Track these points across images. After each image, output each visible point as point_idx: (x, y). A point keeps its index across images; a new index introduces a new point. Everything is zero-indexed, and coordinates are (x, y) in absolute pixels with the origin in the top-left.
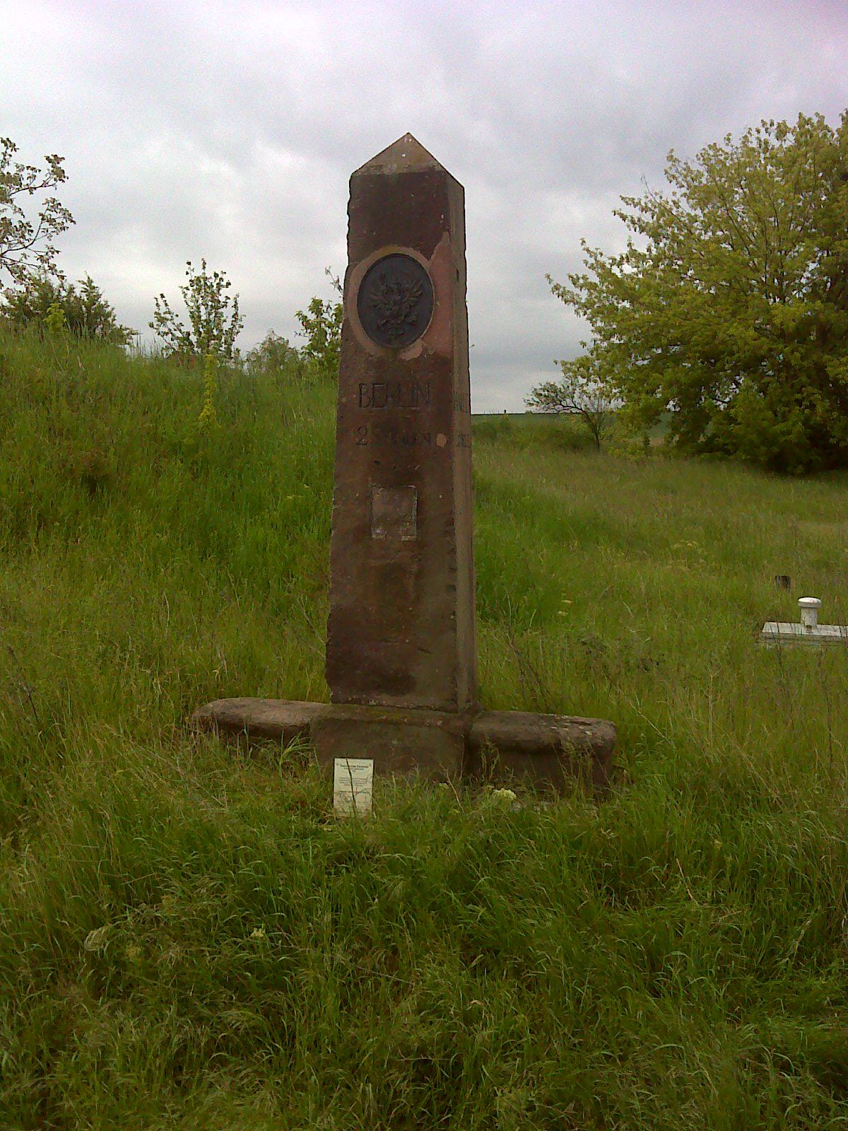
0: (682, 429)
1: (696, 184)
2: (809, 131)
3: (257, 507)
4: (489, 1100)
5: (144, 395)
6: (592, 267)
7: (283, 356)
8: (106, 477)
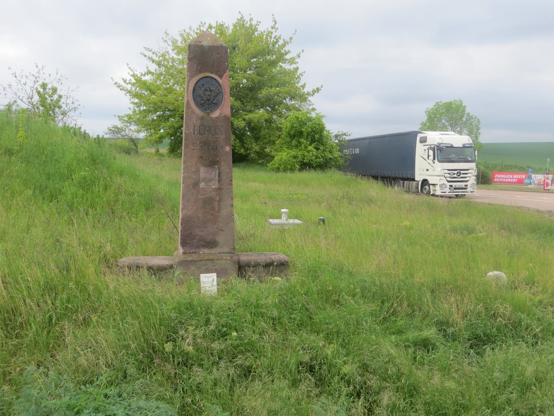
2: (221, 28)
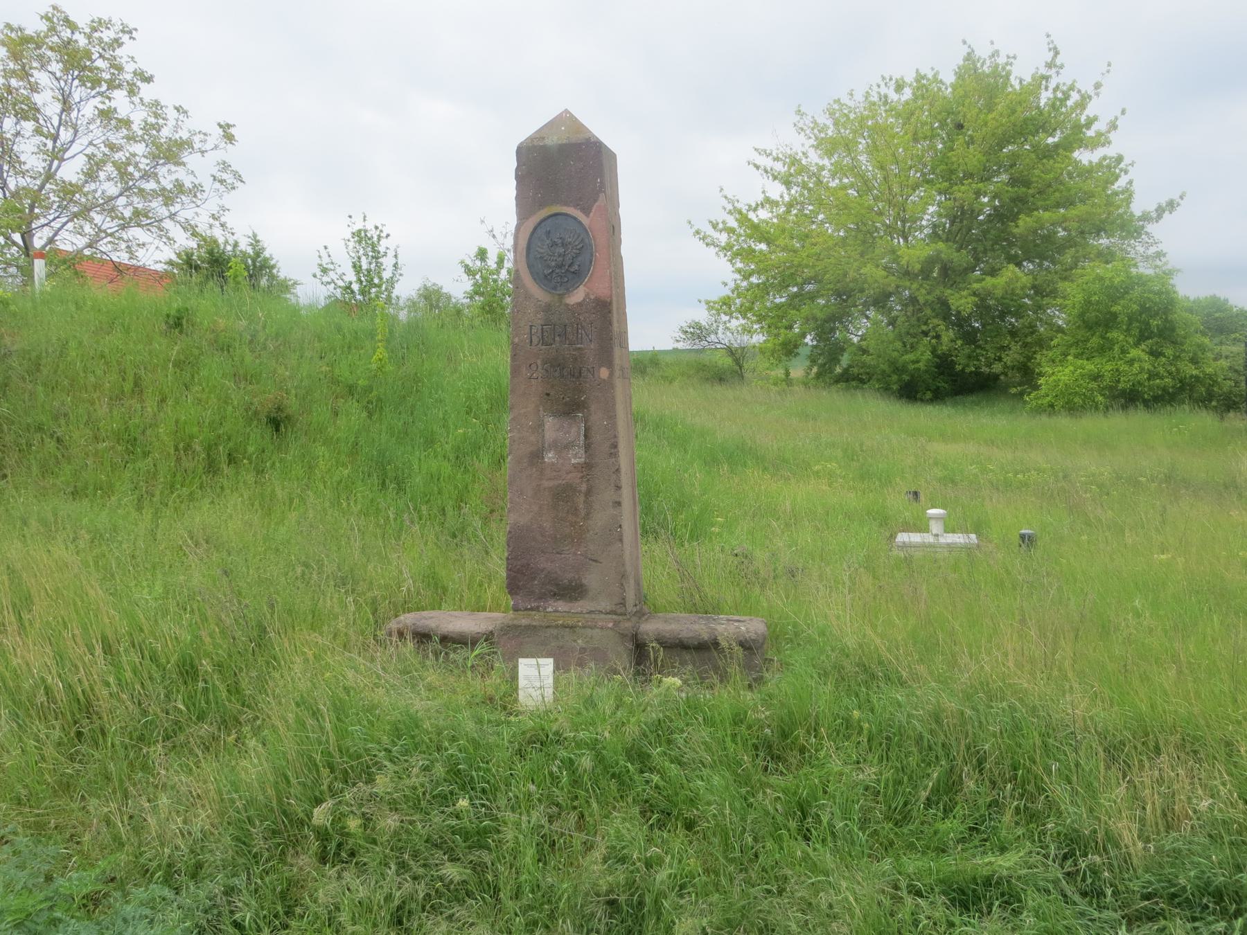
0: (820, 361)
1: (823, 135)
5: (320, 341)
6: (730, 213)
7: (438, 300)
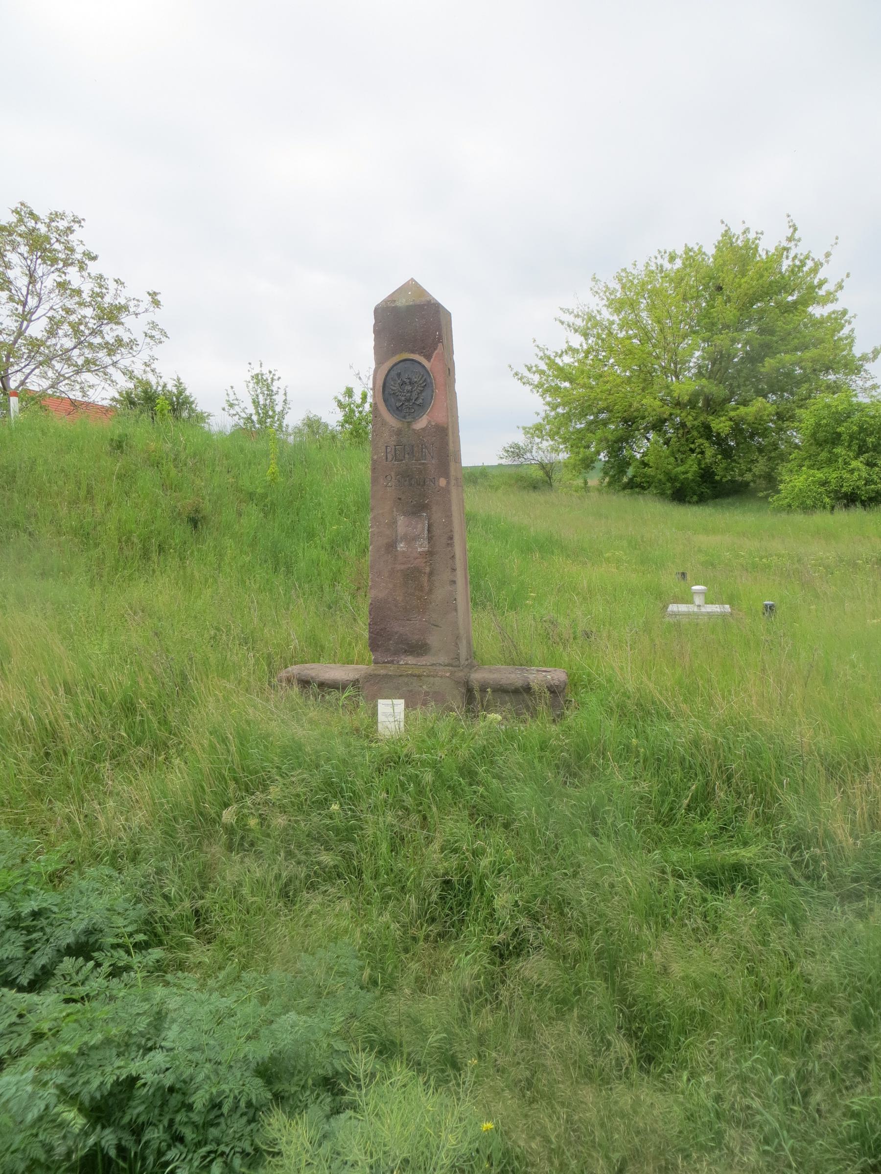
2: (691, 258)
3: (311, 535)
4: (490, 902)
6: (541, 358)
8: (204, 518)
